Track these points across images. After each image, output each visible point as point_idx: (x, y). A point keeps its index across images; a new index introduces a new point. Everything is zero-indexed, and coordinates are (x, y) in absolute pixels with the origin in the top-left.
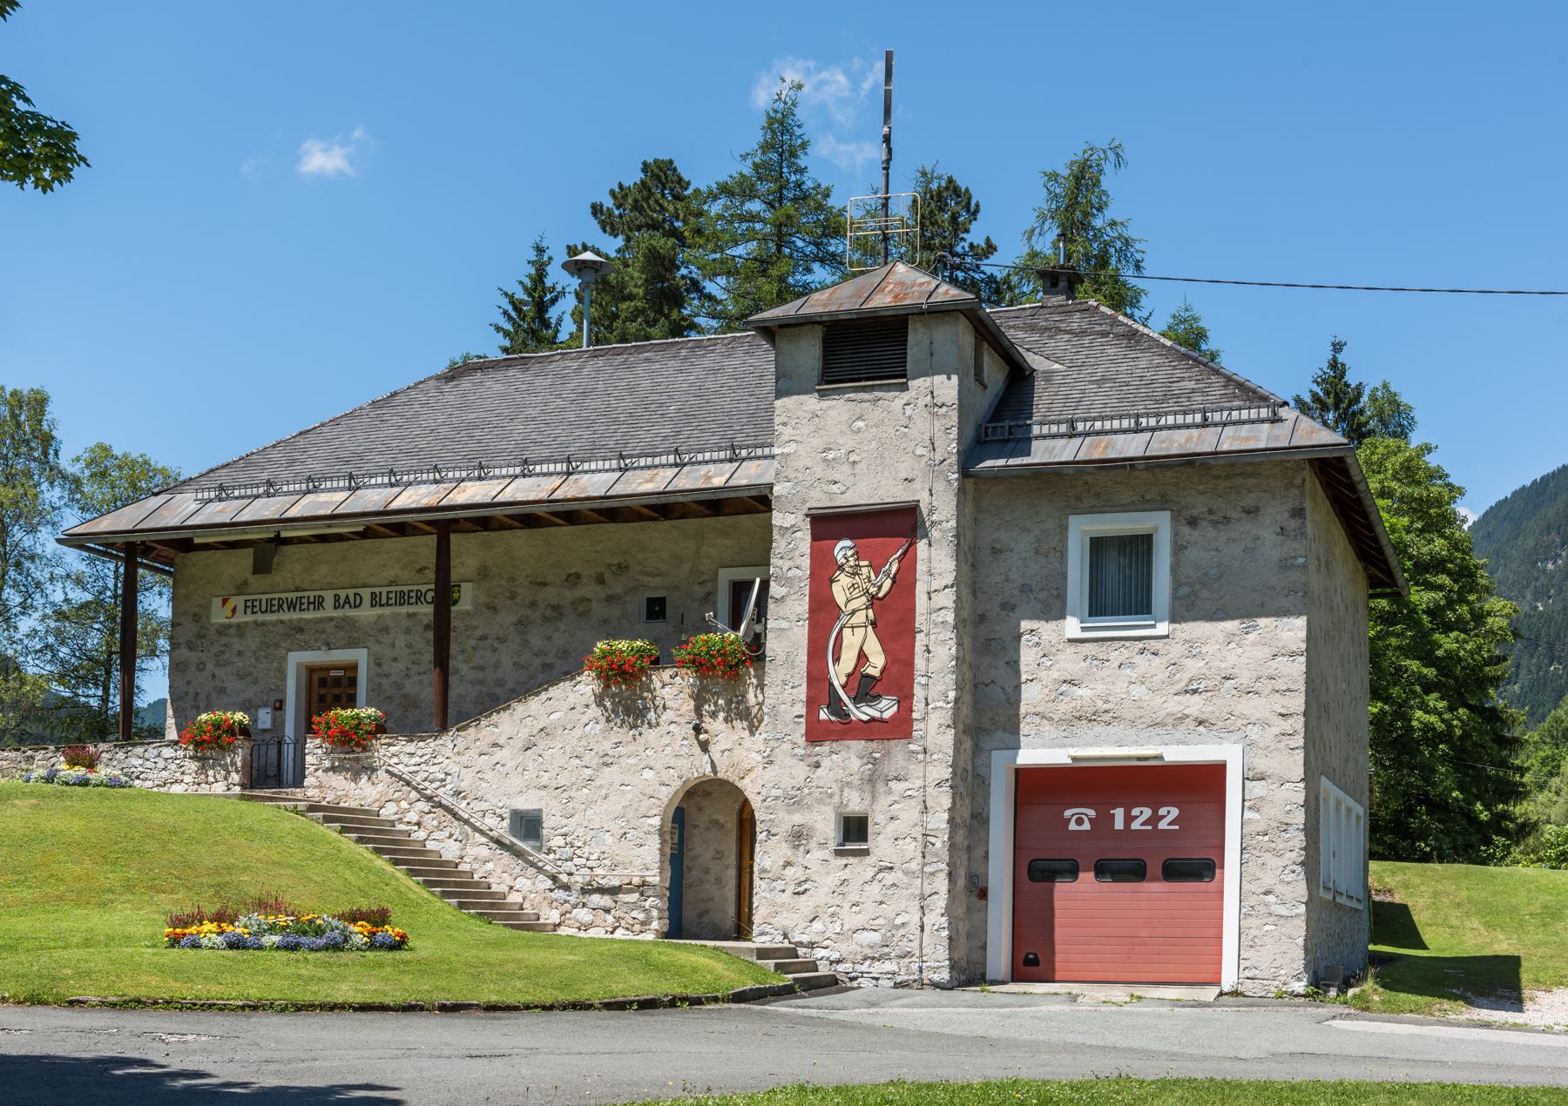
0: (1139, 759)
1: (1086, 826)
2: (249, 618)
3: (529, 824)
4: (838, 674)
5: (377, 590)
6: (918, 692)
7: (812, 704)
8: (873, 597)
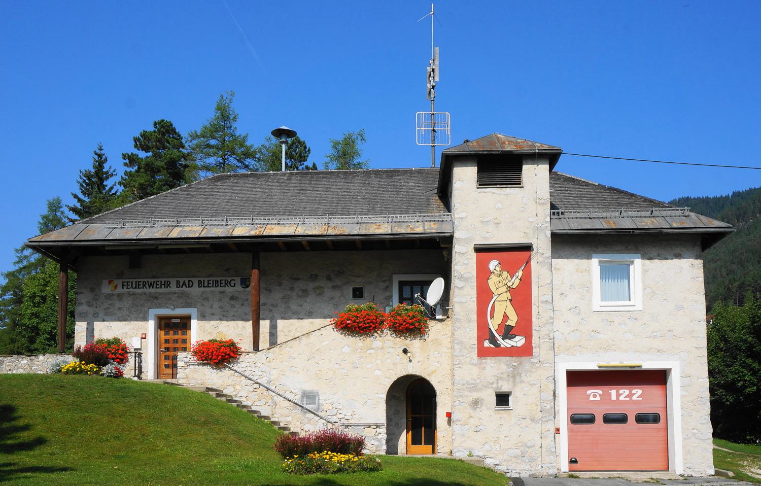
0: (630, 367)
1: (598, 398)
2: (125, 290)
3: (310, 396)
5: (202, 279)
6: (534, 333)
7: (480, 340)
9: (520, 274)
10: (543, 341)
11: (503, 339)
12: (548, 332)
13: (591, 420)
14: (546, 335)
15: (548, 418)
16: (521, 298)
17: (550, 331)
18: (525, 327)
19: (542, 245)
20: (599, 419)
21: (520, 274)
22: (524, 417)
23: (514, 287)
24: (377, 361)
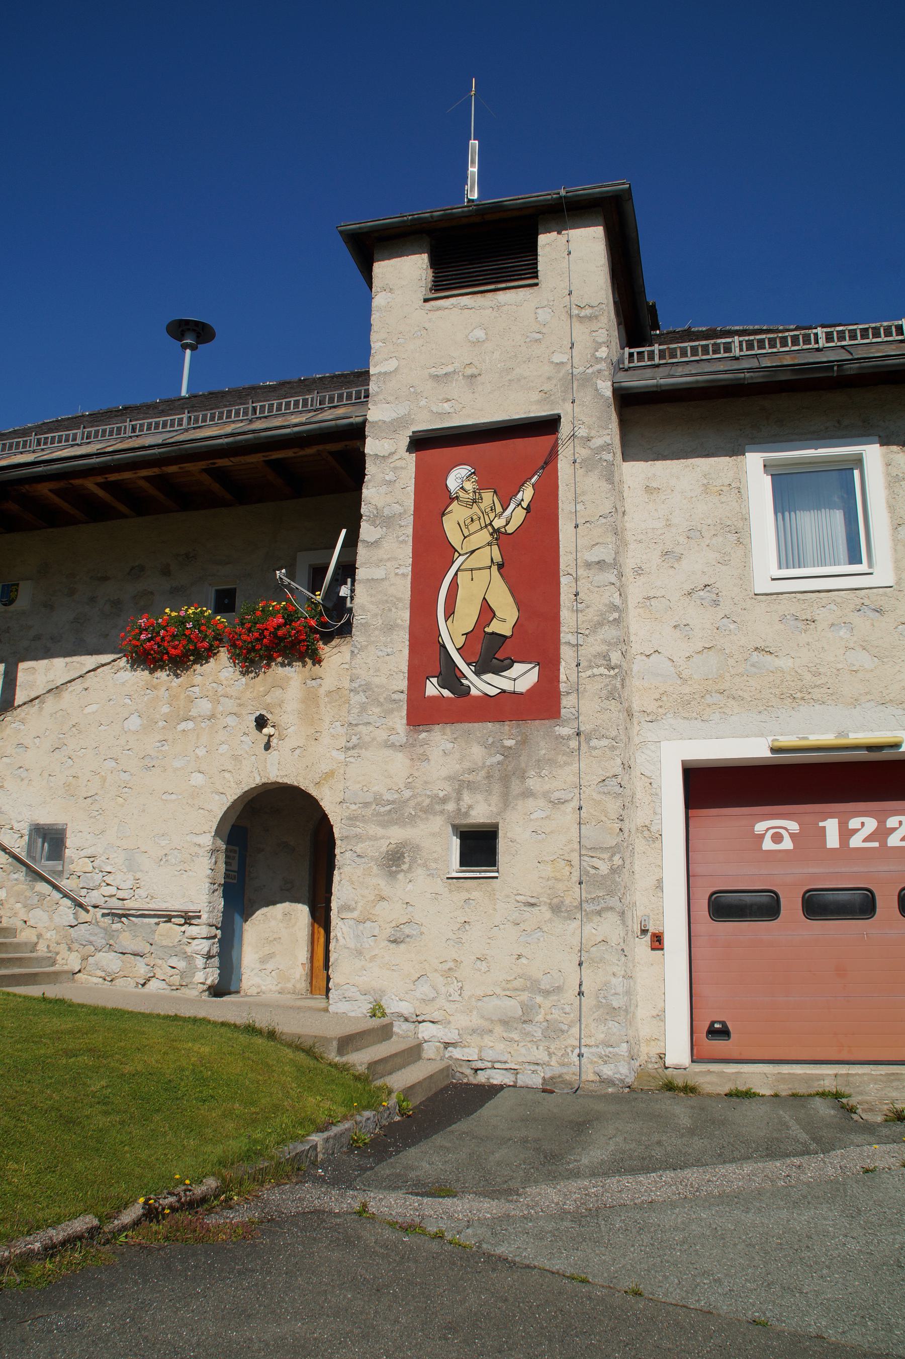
0: (870, 748)
1: (787, 844)
3: (51, 839)
4: (452, 634)
6: (566, 653)
8: (496, 531)
9: (527, 494)
10: (589, 673)
11: (478, 673)
12: (605, 648)
13: (767, 908)
14: (599, 655)
15: (603, 905)
16: (530, 559)
17: (609, 644)
18: (537, 638)
19: (590, 423)
20: (791, 905)
21: (527, 494)
22: (533, 901)
23: (510, 529)
24: (197, 751)
